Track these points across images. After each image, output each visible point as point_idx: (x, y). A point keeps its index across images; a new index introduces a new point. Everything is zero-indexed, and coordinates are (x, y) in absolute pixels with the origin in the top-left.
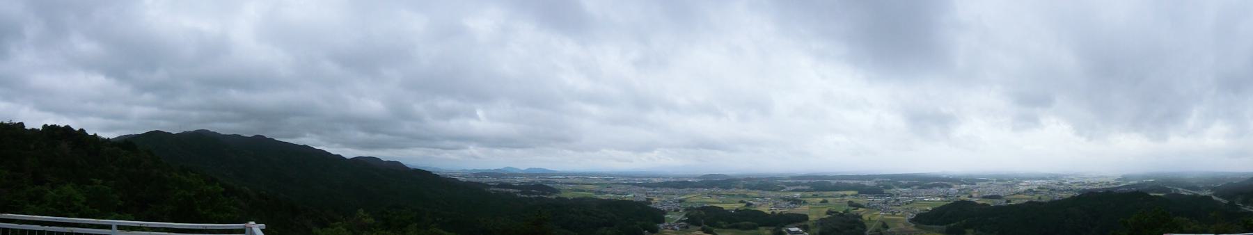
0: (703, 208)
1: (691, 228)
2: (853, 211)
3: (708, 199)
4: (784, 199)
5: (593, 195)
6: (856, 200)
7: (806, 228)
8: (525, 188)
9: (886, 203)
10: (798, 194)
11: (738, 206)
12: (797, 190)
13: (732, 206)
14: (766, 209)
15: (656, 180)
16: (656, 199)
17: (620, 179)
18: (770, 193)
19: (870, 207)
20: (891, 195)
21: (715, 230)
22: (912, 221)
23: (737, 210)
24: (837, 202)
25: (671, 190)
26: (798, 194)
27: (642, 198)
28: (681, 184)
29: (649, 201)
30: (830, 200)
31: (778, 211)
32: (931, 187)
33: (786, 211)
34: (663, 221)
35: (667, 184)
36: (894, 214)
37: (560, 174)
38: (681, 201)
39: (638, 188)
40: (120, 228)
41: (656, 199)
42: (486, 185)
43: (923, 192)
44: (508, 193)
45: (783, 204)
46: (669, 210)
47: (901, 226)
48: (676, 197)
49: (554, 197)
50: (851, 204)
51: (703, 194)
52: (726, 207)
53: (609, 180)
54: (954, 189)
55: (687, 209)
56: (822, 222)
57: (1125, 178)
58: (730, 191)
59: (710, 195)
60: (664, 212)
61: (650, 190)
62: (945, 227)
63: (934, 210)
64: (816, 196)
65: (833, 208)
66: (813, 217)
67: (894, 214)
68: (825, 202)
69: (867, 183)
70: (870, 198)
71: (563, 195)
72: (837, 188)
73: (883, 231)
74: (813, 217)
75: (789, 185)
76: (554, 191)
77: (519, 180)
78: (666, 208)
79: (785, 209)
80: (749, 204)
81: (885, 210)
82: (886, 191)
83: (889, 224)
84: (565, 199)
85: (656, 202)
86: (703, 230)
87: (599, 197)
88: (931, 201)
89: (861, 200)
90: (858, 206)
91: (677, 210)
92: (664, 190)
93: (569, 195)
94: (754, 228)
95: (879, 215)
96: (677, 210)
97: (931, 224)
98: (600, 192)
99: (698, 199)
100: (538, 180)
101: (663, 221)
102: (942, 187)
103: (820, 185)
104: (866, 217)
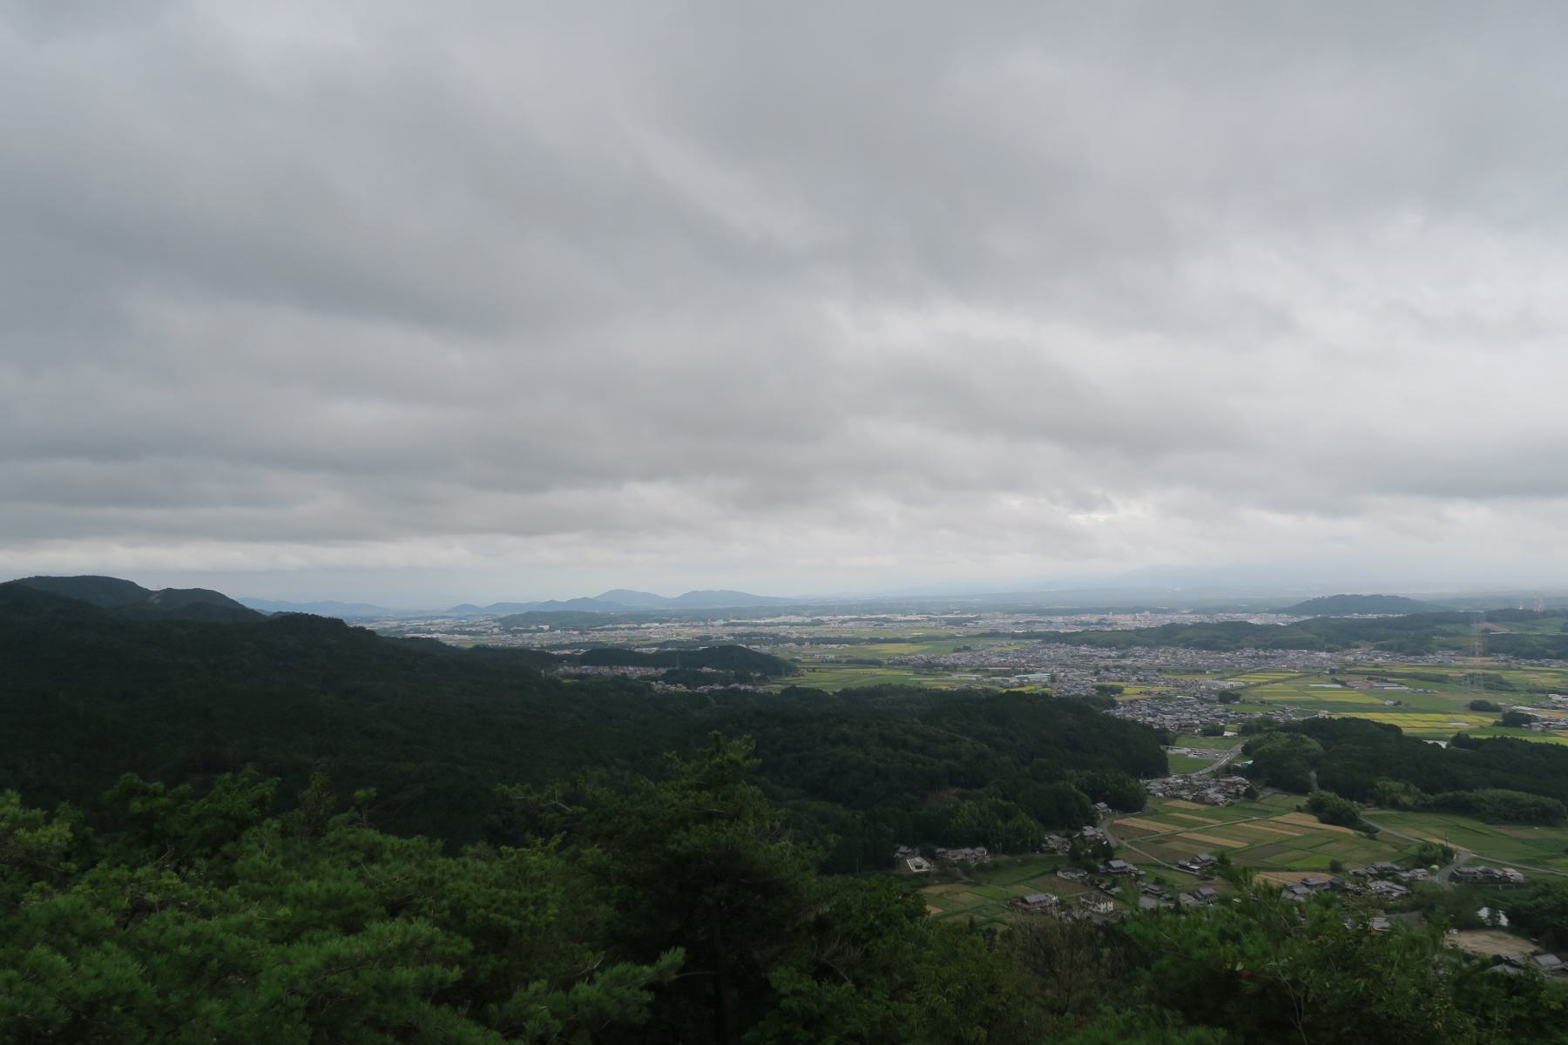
1: (1268, 796)
3: (1332, 692)
8: (684, 661)
11: (1467, 723)
13: (1436, 722)
15: (1126, 621)
16: (1131, 691)
17: (1001, 622)
21: (1367, 813)
23: (1460, 740)
25: (1187, 656)
27: (1080, 683)
28: (1222, 635)
29: (1107, 695)
34: (1159, 767)
35: (1168, 635)
37: (796, 609)
38: (1226, 697)
39: (1063, 651)
41: (1131, 691)
42: (543, 657)
44: (622, 683)
46: (1185, 728)
48: (1210, 682)
49: (775, 688)
52: (1411, 723)
55: (1246, 730)
57: (531, 618)
58: (1426, 665)
59: (1338, 675)
60: (1164, 737)
71: (807, 680)
76: (773, 666)
77: (657, 633)
78: (1169, 721)
84: (816, 695)
85: (1133, 698)
86: (1316, 808)
87: (929, 682)
91: (1213, 731)
92: (1162, 657)
93: (829, 682)
98: (930, 667)
100: (719, 631)
101: (1159, 767)
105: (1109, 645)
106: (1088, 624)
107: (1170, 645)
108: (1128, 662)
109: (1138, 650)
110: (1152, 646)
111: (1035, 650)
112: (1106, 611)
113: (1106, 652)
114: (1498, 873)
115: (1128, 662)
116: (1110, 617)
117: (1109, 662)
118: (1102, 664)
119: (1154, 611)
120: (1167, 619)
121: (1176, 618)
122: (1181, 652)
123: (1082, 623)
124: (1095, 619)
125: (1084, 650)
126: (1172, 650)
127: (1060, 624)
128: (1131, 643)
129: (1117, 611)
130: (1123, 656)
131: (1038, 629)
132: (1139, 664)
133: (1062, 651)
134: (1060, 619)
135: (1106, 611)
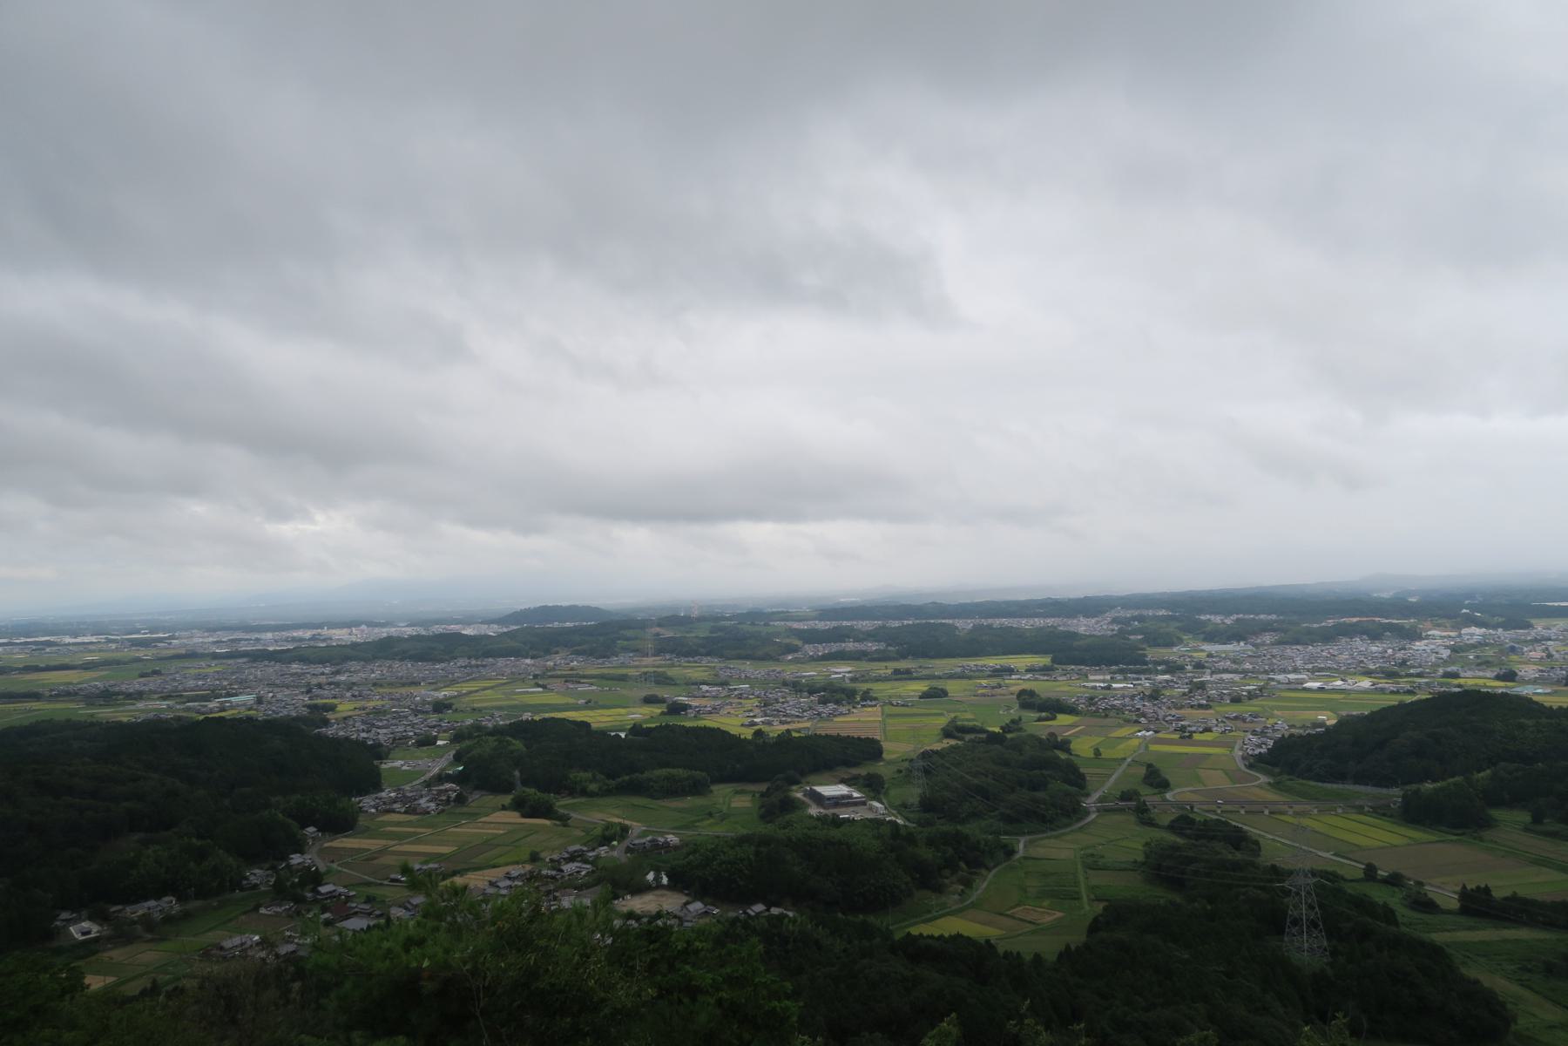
0: (521, 729)
1: (477, 799)
2: (1036, 726)
3: (533, 695)
4: (796, 687)
5: (80, 711)
6: (1045, 688)
7: (874, 786)
9: (1155, 696)
10: (842, 671)
12: (841, 657)
13: (616, 716)
14: (734, 722)
15: (341, 635)
16: (345, 707)
17: (199, 640)
18: (748, 667)
19: (1096, 710)
20: (1173, 668)
21: (561, 803)
22: (1258, 762)
23: (636, 730)
24: (983, 696)
25: (403, 669)
26: (842, 671)
27: (290, 703)
28: (438, 646)
29: (319, 714)
30: (952, 687)
31: (776, 729)
32: (1328, 637)
33: (803, 726)
34: (372, 783)
35: (386, 649)
36: (1186, 735)
38: (440, 707)
39: (272, 670)
40: (138, 632)
41: (345, 707)
43: (1297, 654)
45: (792, 703)
46: (399, 741)
47: (1217, 781)
48: (423, 693)
50: (1028, 700)
51: (517, 678)
52: (598, 719)
53: (148, 651)
54: (1433, 645)
56: (929, 763)
58: (610, 666)
60: (379, 751)
61: (320, 673)
62: (1395, 794)
63: (1343, 723)
64: (905, 675)
65: (967, 717)
66: (896, 749)
67: (1186, 735)
68: (935, 694)
69: (1082, 626)
70: (1097, 680)
72: (975, 645)
73: (1149, 796)
74: (896, 749)
75: (812, 637)
78: (383, 735)
79: (801, 720)
80: (677, 709)
81: (1156, 723)
82: (1152, 653)
83: (1168, 773)
85: (346, 715)
86: (519, 805)
87: (106, 714)
88: (1335, 687)
89: (1062, 686)
90: (1055, 707)
91: (426, 742)
92: (377, 671)
94: (697, 788)
95: (1132, 741)
96: (426, 742)
97: (1341, 777)
98: (107, 696)
99: (499, 696)
101: (372, 783)
102: (1375, 635)
103: (918, 636)
104: (1083, 747)
106: (301, 640)
108: (343, 678)
110: (367, 661)
112: (320, 626)
113: (319, 669)
115: (343, 678)
117: (322, 679)
118: (314, 681)
119: (371, 624)
120: (384, 633)
121: (393, 631)
122: (397, 665)
123: (294, 640)
124: (308, 634)
126: (388, 663)
128: (348, 658)
130: (338, 673)
131: (243, 647)
132: (355, 679)
134: (269, 635)
135: (320, 626)
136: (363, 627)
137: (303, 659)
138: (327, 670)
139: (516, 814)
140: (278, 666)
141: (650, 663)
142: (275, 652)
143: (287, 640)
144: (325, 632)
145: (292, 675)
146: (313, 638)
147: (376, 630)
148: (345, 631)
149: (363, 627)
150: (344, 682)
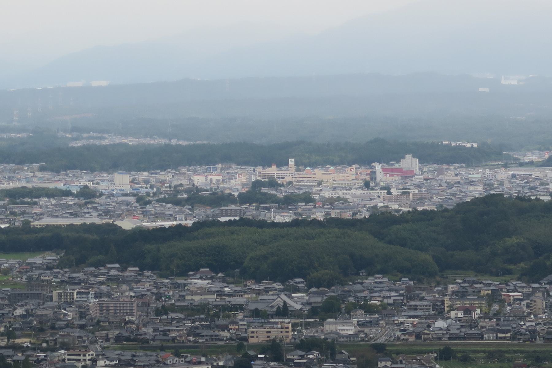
15: (340, 189)
39: (130, 292)
105: (281, 271)
106: (218, 199)
107: (481, 268)
108: (346, 328)
109: (379, 288)
110: (421, 274)
111: (35, 290)
112: (274, 155)
113: (276, 296)
114: (233, 193)
115: (346, 328)
116: (291, 176)
117: (283, 330)
118: (259, 335)
119: (433, 154)
120: (473, 183)
121: (504, 179)
122: (515, 291)
123: (195, 198)
124: (237, 180)
125: (201, 286)
126: (487, 285)
127: (122, 198)
128: (359, 265)
129: (205, 156)
130: (329, 310)
131: (49, 217)
132: (380, 334)
133: (126, 293)
134: (122, 181)
135: (274, 155)
136: (410, 162)
137: (222, 263)
138: (297, 301)
139: (4, 354)
140: (148, 283)
141: (384, 289)
142: (141, 234)
143: (173, 199)
144: (290, 175)
145: (192, 311)
146: (254, 195)
147: (450, 174)
148: (352, 174)
149: (410, 162)
150: (351, 343)
